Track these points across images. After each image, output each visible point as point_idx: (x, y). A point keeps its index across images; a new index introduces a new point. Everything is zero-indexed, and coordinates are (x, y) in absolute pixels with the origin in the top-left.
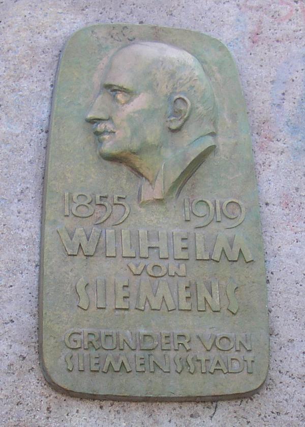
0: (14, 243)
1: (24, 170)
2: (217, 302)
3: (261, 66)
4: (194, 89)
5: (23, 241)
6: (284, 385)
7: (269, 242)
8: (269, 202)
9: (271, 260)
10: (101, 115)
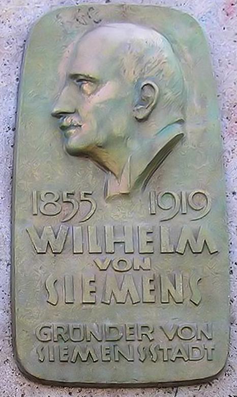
4: (163, 73)
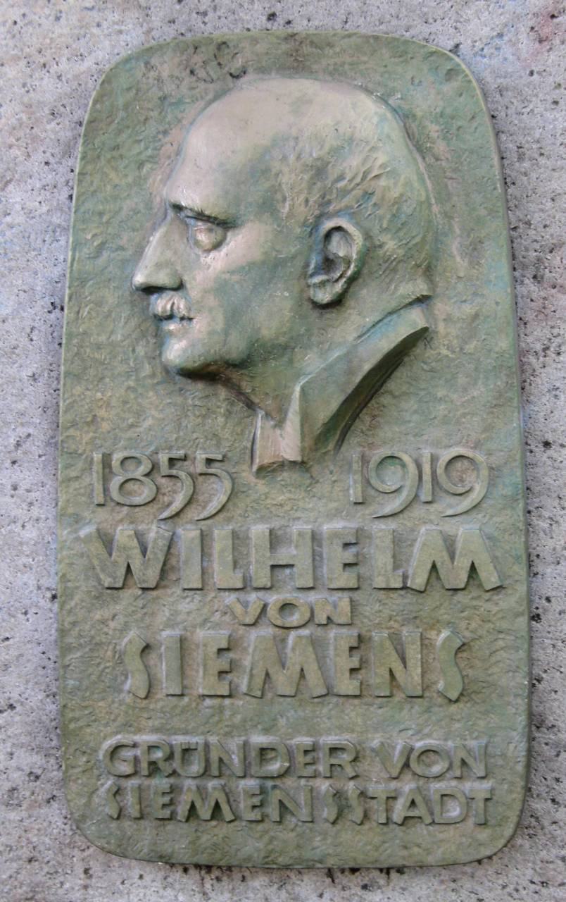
0: (7, 553)
1: (21, 395)
2: (416, 678)
3: (556, 103)
4: (374, 199)
5: (25, 548)
6: (560, 827)
7: (544, 531)
8: (550, 440)
9: (549, 570)
10: (162, 279)
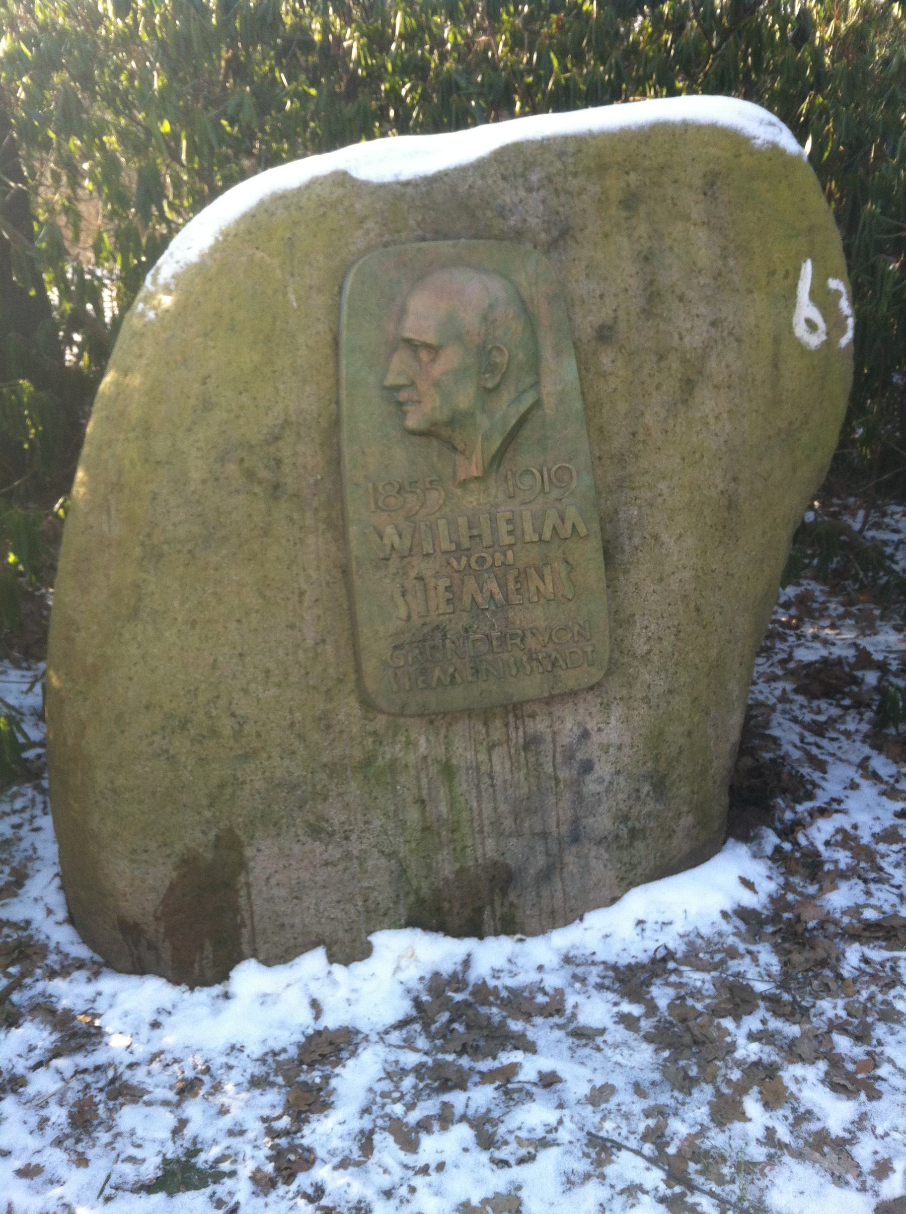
10: (402, 381)
